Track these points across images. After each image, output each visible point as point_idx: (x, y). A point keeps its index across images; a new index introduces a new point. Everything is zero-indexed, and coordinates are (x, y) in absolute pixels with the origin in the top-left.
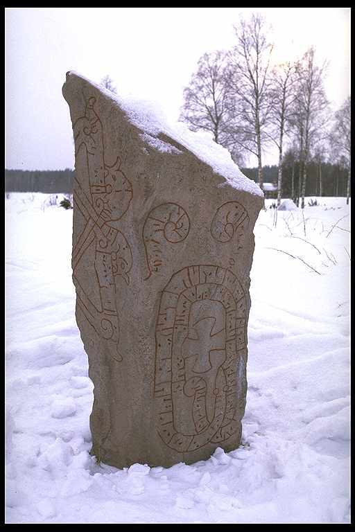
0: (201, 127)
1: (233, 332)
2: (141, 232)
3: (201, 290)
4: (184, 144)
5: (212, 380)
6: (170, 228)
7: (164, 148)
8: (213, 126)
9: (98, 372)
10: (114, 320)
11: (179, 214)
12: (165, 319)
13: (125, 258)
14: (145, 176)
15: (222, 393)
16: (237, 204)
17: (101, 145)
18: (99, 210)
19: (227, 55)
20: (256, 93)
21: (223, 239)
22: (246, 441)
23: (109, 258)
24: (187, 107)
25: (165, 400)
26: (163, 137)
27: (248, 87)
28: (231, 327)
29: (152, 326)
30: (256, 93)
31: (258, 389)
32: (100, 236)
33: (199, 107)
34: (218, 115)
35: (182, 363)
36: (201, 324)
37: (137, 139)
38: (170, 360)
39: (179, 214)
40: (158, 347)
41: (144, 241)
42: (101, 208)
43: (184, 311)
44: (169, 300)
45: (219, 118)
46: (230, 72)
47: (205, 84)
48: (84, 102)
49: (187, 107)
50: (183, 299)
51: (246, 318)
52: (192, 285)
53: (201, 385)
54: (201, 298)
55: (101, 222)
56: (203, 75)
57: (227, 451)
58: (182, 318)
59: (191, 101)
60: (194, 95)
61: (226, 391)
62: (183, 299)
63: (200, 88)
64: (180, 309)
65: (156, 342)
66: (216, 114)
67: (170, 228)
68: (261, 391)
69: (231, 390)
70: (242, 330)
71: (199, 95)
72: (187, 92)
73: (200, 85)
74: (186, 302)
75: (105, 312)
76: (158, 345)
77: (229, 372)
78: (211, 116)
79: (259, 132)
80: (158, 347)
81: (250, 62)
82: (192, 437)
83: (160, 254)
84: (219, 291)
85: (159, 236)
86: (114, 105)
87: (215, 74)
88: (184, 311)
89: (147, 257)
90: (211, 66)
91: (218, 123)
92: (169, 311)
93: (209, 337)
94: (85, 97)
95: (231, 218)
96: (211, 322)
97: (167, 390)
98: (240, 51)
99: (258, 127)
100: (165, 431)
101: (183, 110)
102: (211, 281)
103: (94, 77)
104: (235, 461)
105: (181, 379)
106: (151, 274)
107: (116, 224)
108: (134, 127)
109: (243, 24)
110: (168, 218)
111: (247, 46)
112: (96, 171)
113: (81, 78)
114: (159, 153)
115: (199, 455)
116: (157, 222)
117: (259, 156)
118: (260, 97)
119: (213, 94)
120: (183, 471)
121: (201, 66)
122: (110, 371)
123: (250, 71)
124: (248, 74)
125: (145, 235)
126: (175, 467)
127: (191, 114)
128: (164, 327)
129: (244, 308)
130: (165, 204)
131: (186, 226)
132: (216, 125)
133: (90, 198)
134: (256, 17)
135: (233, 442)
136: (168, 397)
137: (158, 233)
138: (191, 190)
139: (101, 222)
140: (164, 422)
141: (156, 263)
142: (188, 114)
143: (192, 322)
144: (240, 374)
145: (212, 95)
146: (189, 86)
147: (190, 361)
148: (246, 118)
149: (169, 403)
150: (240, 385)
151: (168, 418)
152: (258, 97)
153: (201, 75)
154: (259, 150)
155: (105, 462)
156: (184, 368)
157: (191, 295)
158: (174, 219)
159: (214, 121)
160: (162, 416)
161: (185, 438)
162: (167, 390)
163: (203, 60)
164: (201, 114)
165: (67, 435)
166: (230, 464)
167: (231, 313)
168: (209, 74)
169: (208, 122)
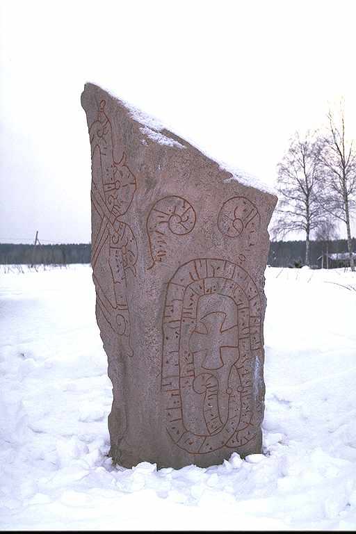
0: (293, 198)
1: (246, 331)
2: (144, 222)
3: (209, 284)
4: (187, 140)
5: (223, 379)
6: (175, 220)
7: (166, 141)
8: (305, 197)
9: (115, 370)
10: (125, 314)
12: (172, 311)
13: (132, 250)
14: (145, 166)
15: (236, 393)
20: (343, 163)
21: (231, 234)
23: (120, 253)
25: (173, 395)
26: (165, 132)
28: (243, 324)
29: (158, 317)
30: (343, 163)
31: (289, 402)
32: (112, 233)
33: (291, 180)
34: (309, 187)
36: (210, 318)
37: (137, 131)
39: (184, 207)
41: (148, 232)
42: (112, 204)
43: (191, 304)
44: (175, 292)
45: (309, 190)
47: (295, 160)
49: (279, 180)
50: (190, 292)
51: (262, 317)
54: (210, 292)
55: (112, 220)
56: (294, 151)
57: (243, 457)
61: (241, 392)
62: (190, 292)
63: (292, 163)
64: (187, 302)
66: (307, 186)
68: (292, 404)
69: (247, 391)
70: (258, 329)
71: (291, 169)
72: (280, 167)
74: (193, 295)
75: (119, 307)
76: (165, 338)
78: (303, 188)
79: (347, 201)
82: (204, 438)
83: (164, 245)
84: (228, 285)
85: (163, 228)
86: (120, 104)
87: (305, 149)
88: (191, 304)
90: (301, 142)
91: (309, 194)
92: (177, 304)
93: (219, 332)
94: (97, 102)
95: (240, 214)
96: (220, 318)
99: (346, 195)
100: (174, 428)
101: (276, 184)
102: (219, 275)
103: (104, 85)
104: (246, 465)
105: (189, 374)
106: (154, 264)
108: (136, 123)
112: (107, 170)
113: (93, 85)
114: (159, 145)
115: (211, 459)
116: (162, 215)
117: (347, 223)
118: (347, 167)
120: (193, 473)
122: (125, 368)
123: (336, 144)
124: (335, 148)
126: (185, 469)
128: (170, 319)
129: (258, 306)
130: (169, 197)
131: (192, 220)
132: (307, 196)
135: (251, 444)
136: (177, 392)
137: (162, 225)
138: (196, 185)
139: (112, 220)
141: (161, 253)
143: (200, 315)
144: (256, 374)
146: (282, 162)
147: (200, 355)
148: (335, 188)
149: (176, 399)
150: (257, 388)
151: (176, 414)
152: (345, 168)
154: (348, 216)
156: (192, 363)
157: (199, 288)
158: (180, 213)
159: (304, 192)
161: (195, 438)
162: (175, 385)
165: (88, 438)
166: (242, 467)
167: (244, 310)
168: (300, 150)
169: (299, 193)
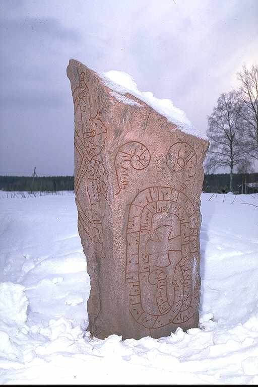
0: (221, 143)
3: (160, 205)
5: (171, 273)
6: (135, 159)
8: (229, 142)
10: (99, 227)
11: (142, 149)
12: (133, 225)
15: (179, 284)
16: (186, 144)
17: (89, 103)
18: (88, 149)
19: (237, 95)
21: (176, 169)
22: (203, 325)
24: (211, 130)
26: (128, 95)
27: (251, 115)
34: (232, 135)
35: (147, 258)
38: (137, 255)
39: (142, 149)
40: (129, 246)
43: (147, 220)
45: (233, 137)
46: (240, 106)
48: (78, 77)
50: (146, 210)
52: (152, 201)
53: (162, 276)
57: (185, 330)
58: (146, 225)
59: (213, 127)
60: (216, 122)
61: (183, 283)
63: (220, 117)
64: (144, 220)
65: (127, 241)
66: (231, 134)
67: (135, 159)
73: (220, 116)
75: (95, 222)
76: (128, 244)
77: (184, 268)
80: (129, 246)
81: (252, 98)
83: (127, 177)
85: (127, 165)
88: (147, 220)
89: (117, 178)
92: (137, 220)
95: (182, 154)
97: (136, 278)
98: (245, 90)
106: (120, 190)
107: (98, 158)
109: (246, 73)
110: (133, 152)
111: (250, 87)
115: (161, 332)
119: (229, 121)
121: (220, 103)
125: (117, 162)
126: (143, 339)
127: (214, 135)
129: (196, 221)
131: (148, 159)
132: (231, 142)
133: (83, 141)
134: (255, 67)
140: (134, 303)
141: (125, 183)
142: (212, 135)
143: (154, 228)
145: (228, 122)
147: (153, 257)
151: (136, 300)
153: (220, 109)
155: (96, 336)
157: (153, 208)
160: (132, 298)
163: (221, 99)
164: (221, 134)
